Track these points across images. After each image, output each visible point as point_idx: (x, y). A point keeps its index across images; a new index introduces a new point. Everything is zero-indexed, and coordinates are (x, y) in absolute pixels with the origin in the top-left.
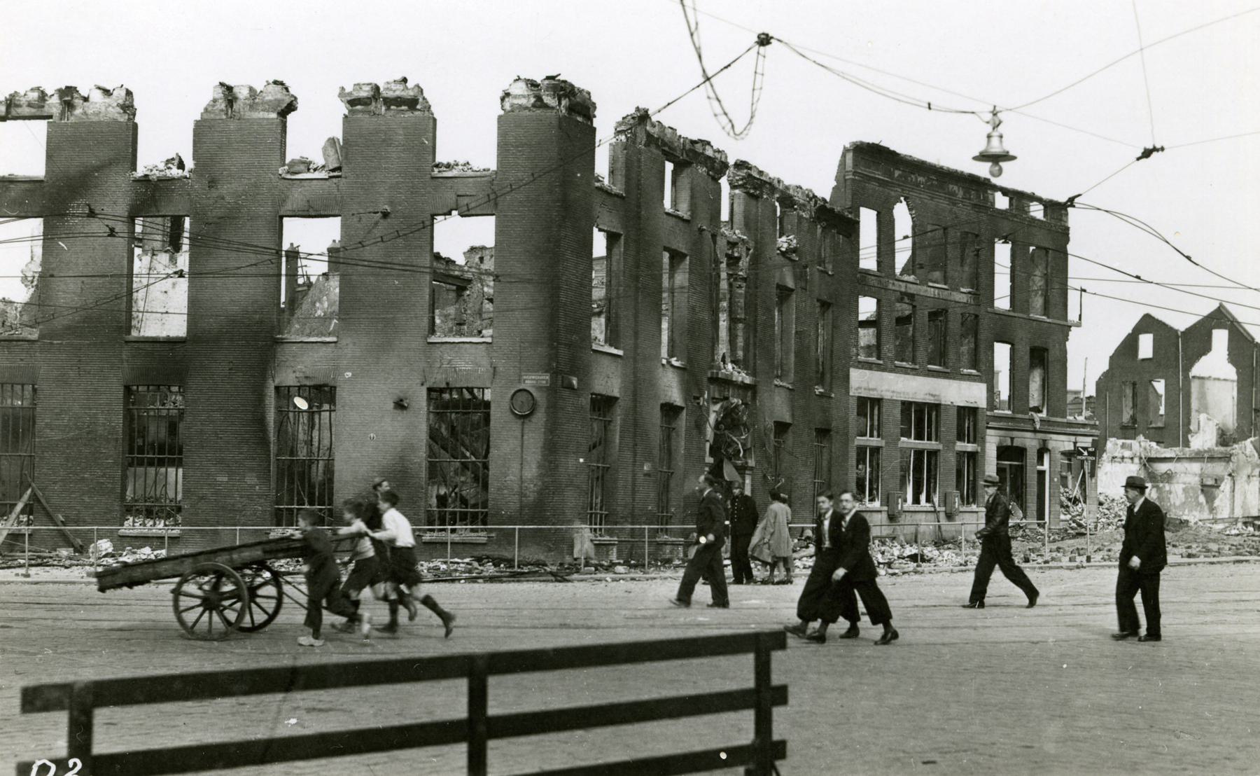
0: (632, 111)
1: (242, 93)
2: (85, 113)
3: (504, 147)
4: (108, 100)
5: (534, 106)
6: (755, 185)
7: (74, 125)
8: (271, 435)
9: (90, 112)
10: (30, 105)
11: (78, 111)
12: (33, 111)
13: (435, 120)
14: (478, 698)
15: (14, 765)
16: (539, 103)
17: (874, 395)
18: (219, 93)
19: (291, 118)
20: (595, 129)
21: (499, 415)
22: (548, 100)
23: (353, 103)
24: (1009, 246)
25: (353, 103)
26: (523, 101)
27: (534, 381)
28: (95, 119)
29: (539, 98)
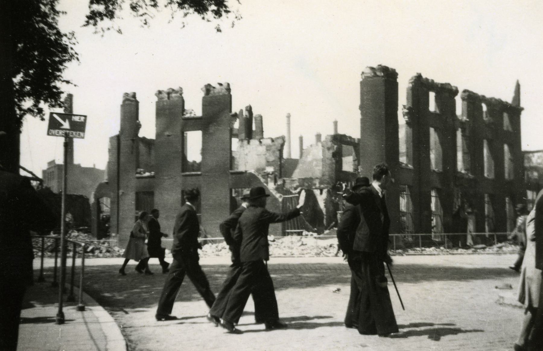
0: (415, 74)
2: (214, 93)
4: (222, 87)
5: (374, 76)
6: (472, 100)
7: (211, 97)
9: (216, 92)
11: (212, 92)
15: (218, 225)
16: (376, 75)
20: (397, 83)
24: (141, 134)
26: (369, 75)
28: (217, 94)
29: (375, 73)
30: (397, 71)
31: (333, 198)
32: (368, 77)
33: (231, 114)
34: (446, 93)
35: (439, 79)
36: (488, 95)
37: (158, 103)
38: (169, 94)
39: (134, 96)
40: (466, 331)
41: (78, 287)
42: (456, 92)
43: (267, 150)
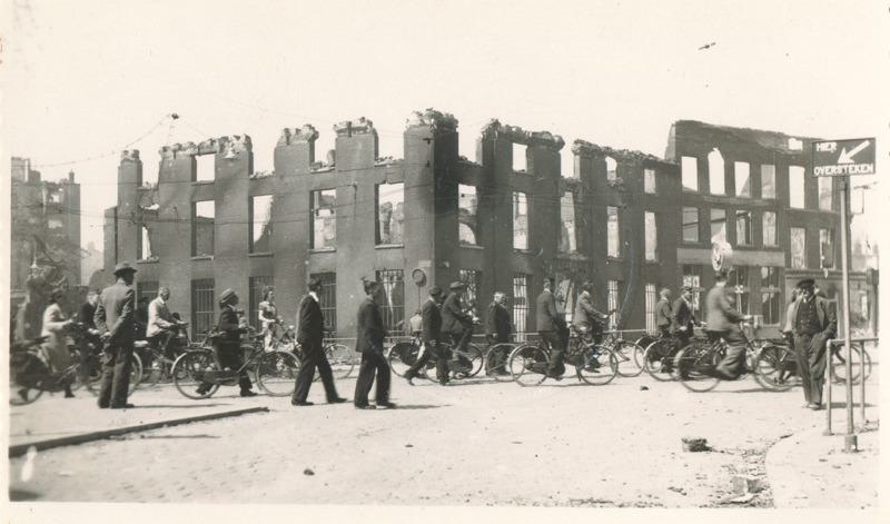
1: (293, 132)
3: (407, 147)
6: (591, 156)
8: (390, 301)
10: (208, 147)
12: (208, 150)
13: (375, 133)
16: (423, 124)
17: (699, 262)
18: (284, 134)
19: (316, 142)
21: (832, 300)
22: (427, 122)
23: (339, 132)
25: (339, 132)
27: (425, 265)
30: (456, 117)
31: (763, 363)
32: (415, 126)
34: (544, 148)
35: (530, 126)
36: (616, 147)
37: (162, 165)
38: (175, 151)
39: (136, 154)
41: (102, 372)
42: (561, 144)
43: (326, 225)
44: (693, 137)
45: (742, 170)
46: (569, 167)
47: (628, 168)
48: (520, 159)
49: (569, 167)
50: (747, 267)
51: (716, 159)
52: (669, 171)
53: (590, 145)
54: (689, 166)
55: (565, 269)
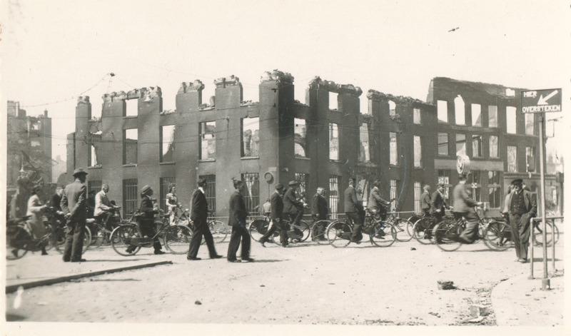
1: (188, 85)
3: (261, 94)
6: (379, 100)
10: (133, 94)
12: (134, 96)
13: (240, 85)
14: (550, 260)
16: (271, 80)
17: (448, 168)
18: (182, 86)
19: (203, 91)
22: (274, 78)
23: (218, 84)
25: (218, 84)
27: (273, 170)
30: (292, 75)
32: (266, 81)
33: (480, 186)
34: (349, 95)
35: (340, 81)
36: (395, 94)
37: (104, 106)
38: (112, 97)
39: (87, 99)
40: (258, 261)
41: (65, 238)
42: (360, 92)
43: (209, 144)
44: (445, 88)
45: (476, 109)
46: (365, 107)
47: (403, 108)
48: (333, 102)
49: (365, 107)
50: (479, 171)
51: (459, 102)
52: (429, 110)
53: (379, 93)
54: (442, 106)
55: (363, 173)
